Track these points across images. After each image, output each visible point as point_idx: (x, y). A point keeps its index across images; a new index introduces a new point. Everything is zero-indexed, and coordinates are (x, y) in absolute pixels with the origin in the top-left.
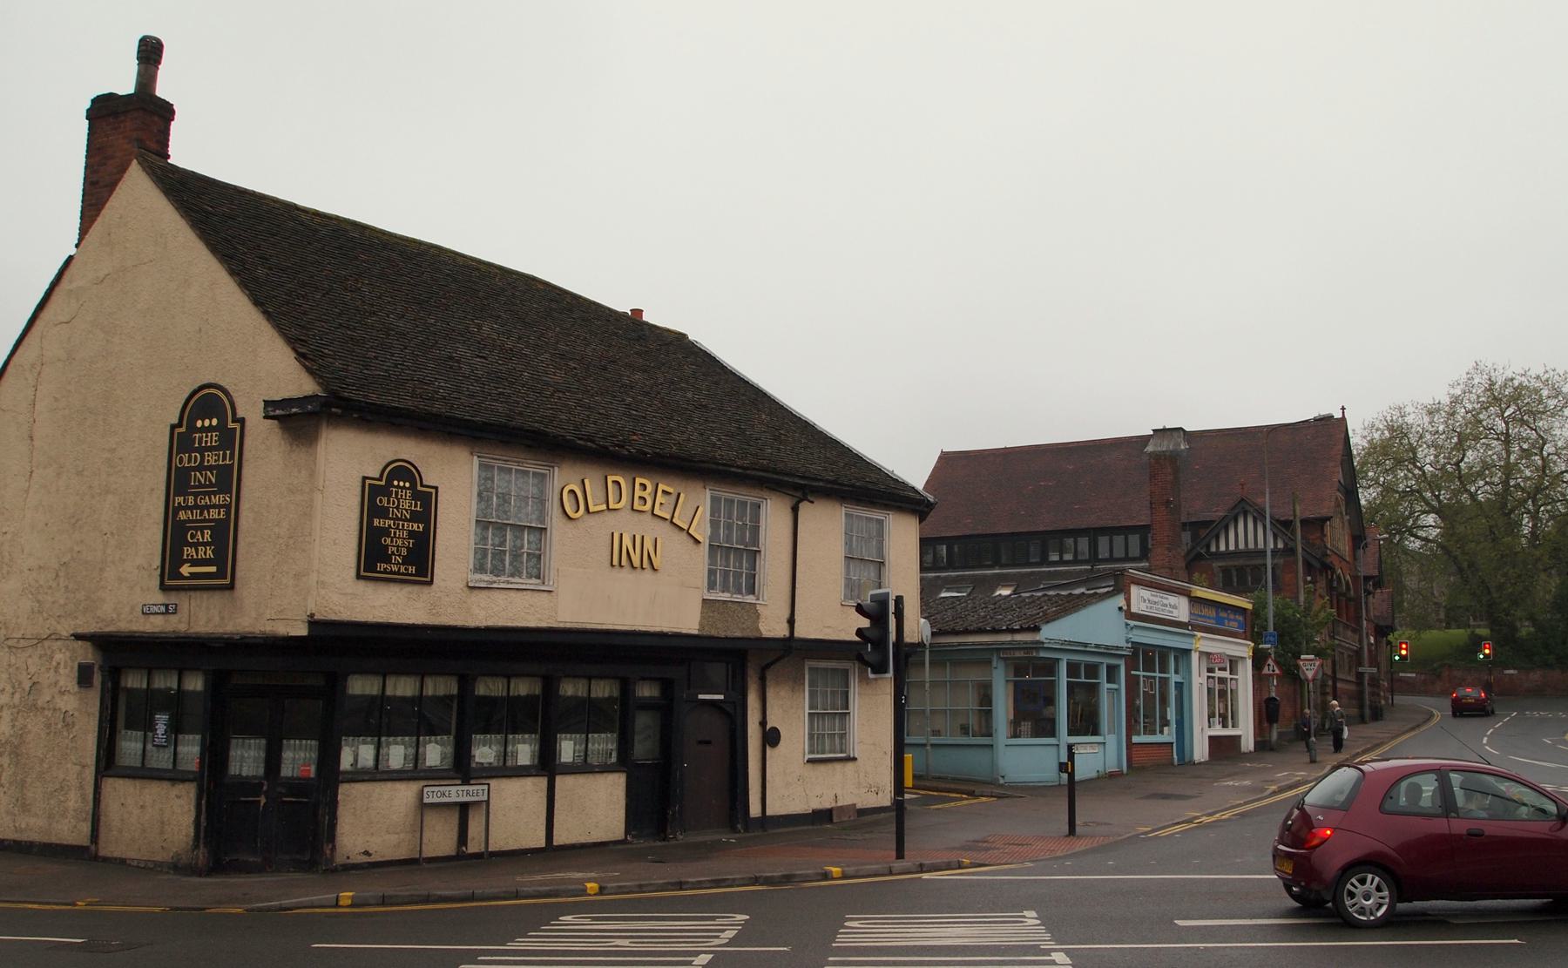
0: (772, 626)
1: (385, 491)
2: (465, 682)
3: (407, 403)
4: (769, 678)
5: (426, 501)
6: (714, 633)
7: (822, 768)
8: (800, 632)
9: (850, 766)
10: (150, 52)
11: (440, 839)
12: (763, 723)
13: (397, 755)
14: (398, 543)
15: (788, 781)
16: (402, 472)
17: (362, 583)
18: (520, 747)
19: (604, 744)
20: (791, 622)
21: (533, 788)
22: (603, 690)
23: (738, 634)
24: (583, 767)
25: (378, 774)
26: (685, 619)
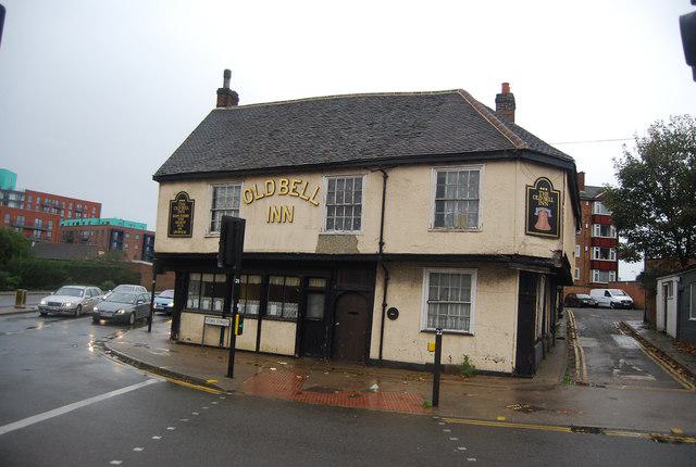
2: (266, 279)
3: (321, 160)
4: (391, 277)
5: (190, 205)
8: (386, 250)
10: (227, 74)
11: (213, 339)
12: (384, 305)
13: (206, 304)
14: (180, 223)
16: (183, 196)
18: (316, 315)
19: (292, 309)
20: (382, 244)
22: (293, 282)
23: (343, 252)
24: (280, 318)
25: (199, 311)
26: (309, 245)
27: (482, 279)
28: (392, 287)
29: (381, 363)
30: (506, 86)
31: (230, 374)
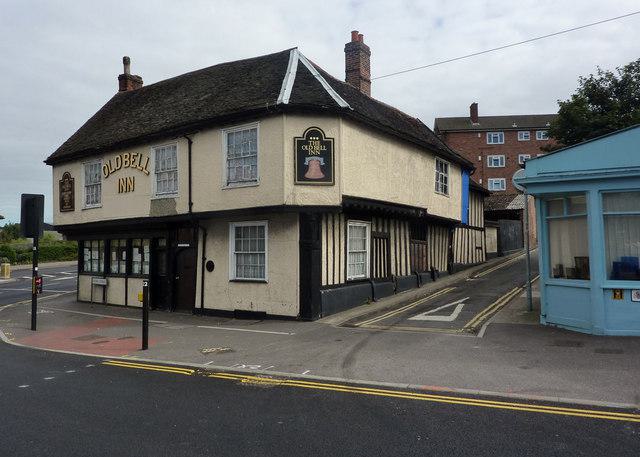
0: (182, 209)
1: (306, 143)
5: (72, 183)
6: (156, 215)
7: (241, 285)
9: (263, 286)
10: (126, 61)
12: (204, 259)
15: (218, 288)
16: (314, 133)
17: (298, 188)
20: (191, 204)
21: (121, 281)
26: (143, 210)
27: (273, 229)
28: (209, 244)
29: (109, 305)
30: (354, 33)
31: (145, 346)
